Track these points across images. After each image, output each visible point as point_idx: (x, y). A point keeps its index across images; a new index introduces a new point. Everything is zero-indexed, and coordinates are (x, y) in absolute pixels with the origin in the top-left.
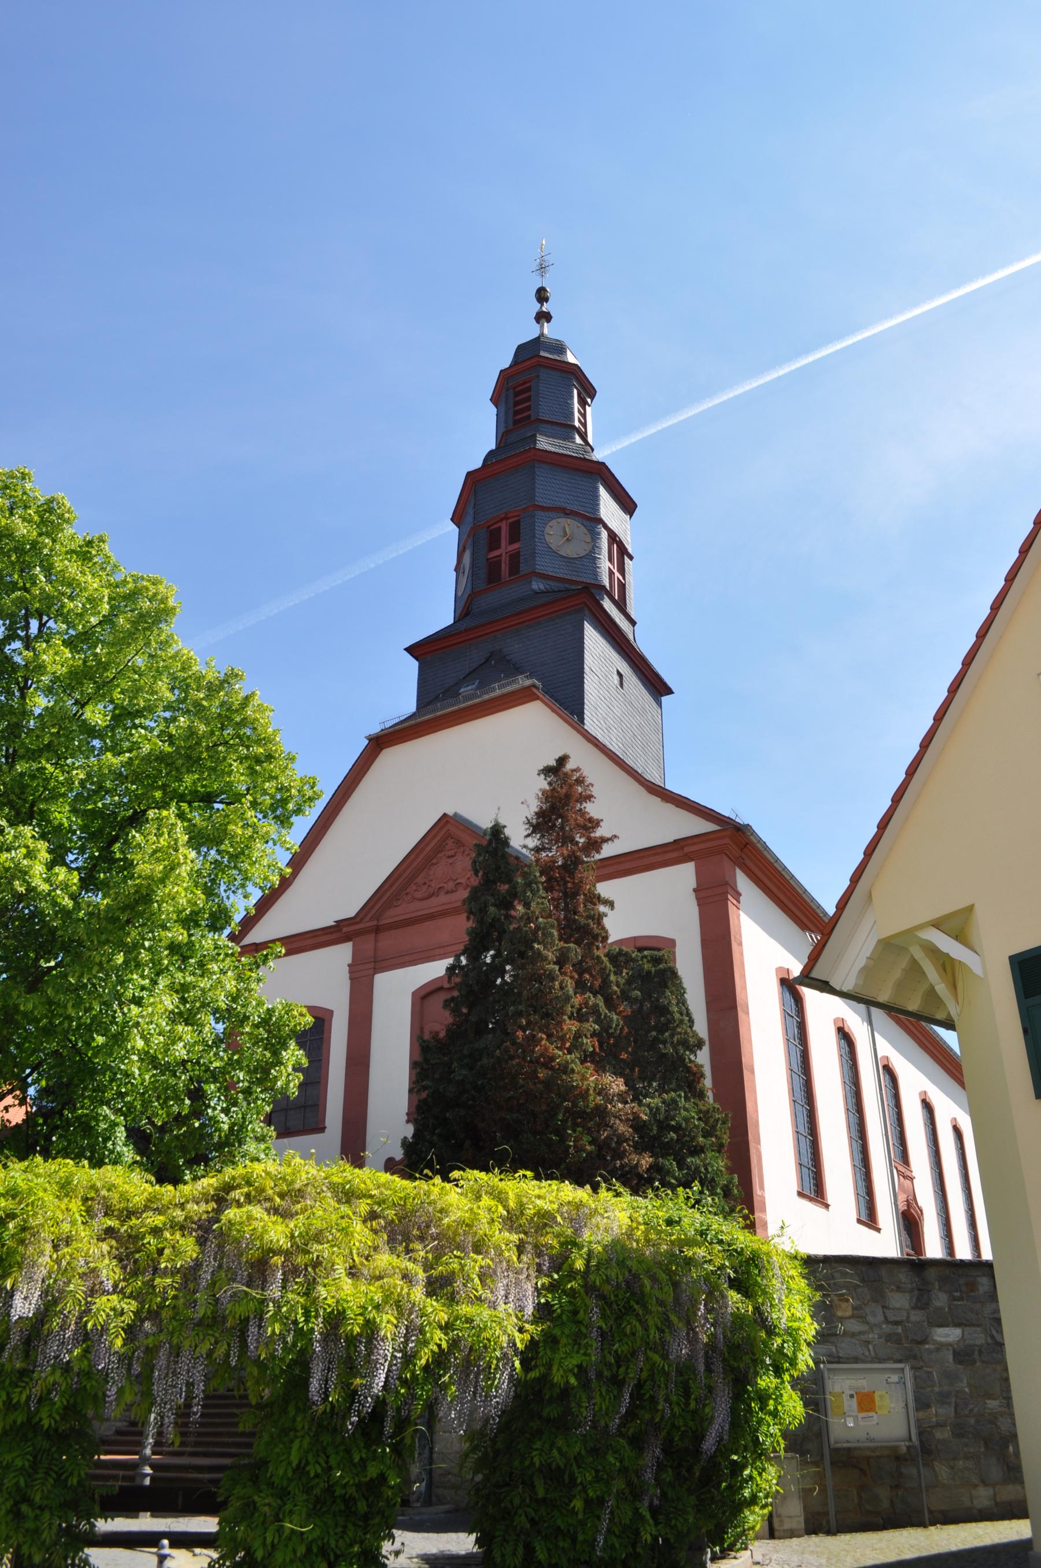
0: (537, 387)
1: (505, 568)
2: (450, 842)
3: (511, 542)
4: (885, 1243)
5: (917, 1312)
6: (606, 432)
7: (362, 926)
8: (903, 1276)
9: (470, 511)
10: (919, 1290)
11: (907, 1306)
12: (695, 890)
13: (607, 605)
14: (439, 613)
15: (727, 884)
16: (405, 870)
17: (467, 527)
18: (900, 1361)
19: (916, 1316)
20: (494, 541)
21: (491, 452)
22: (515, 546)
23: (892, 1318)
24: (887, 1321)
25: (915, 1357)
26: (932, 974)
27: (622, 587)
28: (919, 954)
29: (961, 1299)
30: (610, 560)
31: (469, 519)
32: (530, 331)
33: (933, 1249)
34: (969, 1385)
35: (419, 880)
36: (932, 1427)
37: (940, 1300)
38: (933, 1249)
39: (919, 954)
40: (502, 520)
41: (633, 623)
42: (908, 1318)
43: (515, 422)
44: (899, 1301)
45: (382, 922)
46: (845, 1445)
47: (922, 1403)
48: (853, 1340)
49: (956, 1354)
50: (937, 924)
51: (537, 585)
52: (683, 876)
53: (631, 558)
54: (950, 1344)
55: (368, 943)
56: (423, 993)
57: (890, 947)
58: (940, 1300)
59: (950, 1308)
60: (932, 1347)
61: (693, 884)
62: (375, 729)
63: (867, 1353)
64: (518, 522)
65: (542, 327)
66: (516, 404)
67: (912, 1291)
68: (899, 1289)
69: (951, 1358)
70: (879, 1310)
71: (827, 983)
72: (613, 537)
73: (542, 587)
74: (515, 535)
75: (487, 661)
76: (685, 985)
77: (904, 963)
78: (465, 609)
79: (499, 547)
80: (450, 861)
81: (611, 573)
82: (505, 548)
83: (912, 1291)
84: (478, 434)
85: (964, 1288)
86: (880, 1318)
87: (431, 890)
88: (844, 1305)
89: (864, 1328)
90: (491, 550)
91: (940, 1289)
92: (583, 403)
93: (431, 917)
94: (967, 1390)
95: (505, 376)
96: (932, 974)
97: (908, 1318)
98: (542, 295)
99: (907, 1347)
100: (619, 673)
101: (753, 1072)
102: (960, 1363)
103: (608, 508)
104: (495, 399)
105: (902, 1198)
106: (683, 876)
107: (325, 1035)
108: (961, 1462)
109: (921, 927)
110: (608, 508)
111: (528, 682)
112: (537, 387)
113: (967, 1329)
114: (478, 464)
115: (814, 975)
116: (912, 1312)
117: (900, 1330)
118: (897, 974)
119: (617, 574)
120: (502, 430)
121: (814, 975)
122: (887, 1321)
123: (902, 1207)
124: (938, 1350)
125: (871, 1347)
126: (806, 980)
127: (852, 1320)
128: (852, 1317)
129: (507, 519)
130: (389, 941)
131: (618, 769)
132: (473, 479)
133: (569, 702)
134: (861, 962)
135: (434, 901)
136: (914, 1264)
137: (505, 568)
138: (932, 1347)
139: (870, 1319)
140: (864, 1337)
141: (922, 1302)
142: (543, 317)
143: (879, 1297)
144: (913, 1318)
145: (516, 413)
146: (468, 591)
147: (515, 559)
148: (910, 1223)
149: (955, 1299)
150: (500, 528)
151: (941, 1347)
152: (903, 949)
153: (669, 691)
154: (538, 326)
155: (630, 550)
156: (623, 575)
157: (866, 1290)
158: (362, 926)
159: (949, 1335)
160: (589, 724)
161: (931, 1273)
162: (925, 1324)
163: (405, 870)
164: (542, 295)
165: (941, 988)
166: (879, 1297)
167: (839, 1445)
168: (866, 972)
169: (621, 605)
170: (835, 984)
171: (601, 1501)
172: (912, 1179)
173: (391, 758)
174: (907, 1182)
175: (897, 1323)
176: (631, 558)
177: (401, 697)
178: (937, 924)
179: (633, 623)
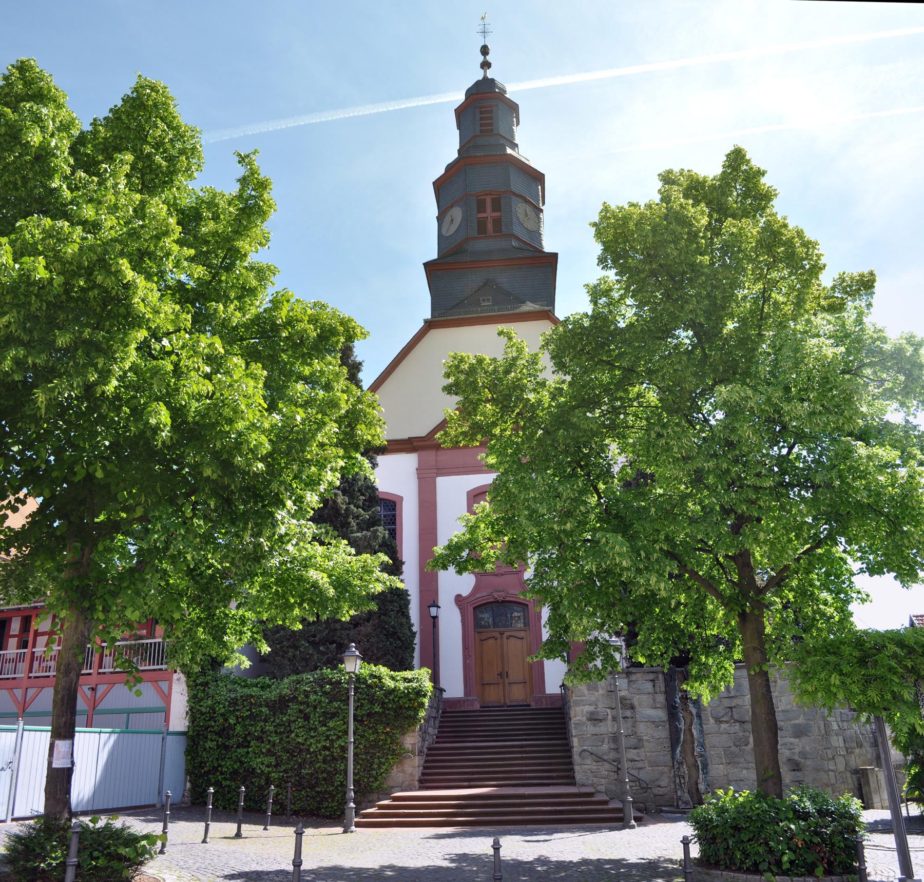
0: (485, 111)
1: (490, 226)
6: (530, 144)
32: (479, 75)
40: (486, 195)
43: (481, 131)
51: (514, 243)
55: (430, 455)
65: (485, 72)
76: (568, 860)
82: (489, 214)
98: (485, 50)
107: (397, 512)
112: (485, 111)
130: (445, 458)
137: (490, 226)
142: (486, 65)
147: (497, 222)
154: (482, 71)
164: (485, 50)
171: (826, 662)
177: (420, 304)
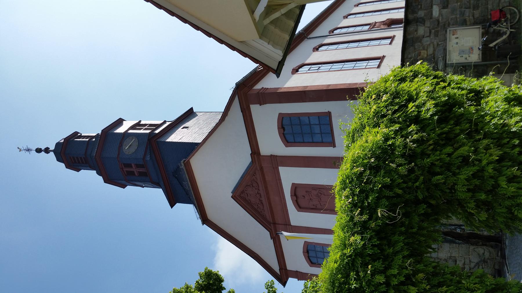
1: (141, 170)
2: (242, 195)
3: (132, 167)
4: (399, 33)
5: (426, 23)
6: (92, 129)
7: (273, 230)
8: (411, 28)
9: (120, 181)
10: (417, 22)
11: (424, 27)
12: (260, 105)
13: (157, 131)
14: (157, 195)
15: (258, 93)
16: (252, 212)
17: (127, 183)
18: (446, 31)
19: (428, 24)
20: (132, 173)
21: (97, 173)
22: (133, 165)
23: (428, 34)
24: (429, 36)
25: (444, 25)
26: (277, 15)
27: (151, 125)
28: (267, 21)
29: (421, 5)
30: (141, 129)
31: (124, 182)
33: (400, 15)
34: (457, 2)
35: (256, 207)
36: (474, 19)
37: (421, 14)
38: (400, 15)
39: (267, 21)
41: (165, 122)
42: (428, 27)
44: (421, 30)
45: (272, 222)
46: (481, 55)
47: (464, 23)
48: (437, 50)
49: (444, 8)
50: (252, 12)
51: (148, 158)
52: (255, 109)
53: (140, 121)
54: (440, 10)
56: (299, 208)
57: (263, 33)
58: (421, 14)
59: (425, 10)
60: (440, 18)
61: (258, 106)
62: (200, 221)
63: (442, 45)
64: (124, 164)
66: (79, 162)
67: (417, 25)
68: (416, 31)
69: (445, 10)
70: (425, 39)
71: (280, 62)
72: (133, 127)
73: (149, 156)
74: (130, 166)
75: (176, 178)
77: (272, 27)
78: (156, 184)
79: (133, 172)
80: (249, 195)
81: (146, 129)
83: (417, 25)
84: (90, 177)
85: (417, 4)
86: (428, 39)
87: (260, 203)
88: (422, 54)
89: (432, 45)
90: (135, 175)
91: (417, 13)
92: (81, 137)
93: (270, 204)
94: (459, 4)
95: (68, 167)
96: (277, 15)
97: (428, 27)
99: (441, 29)
100: (183, 128)
101: (329, 85)
102: (448, 6)
103: (121, 130)
104: (78, 170)
105: (382, 27)
106: (255, 109)
108: (489, 7)
109: (254, 20)
110: (121, 130)
111: (183, 164)
113: (433, 3)
114: (101, 178)
115: (275, 68)
116: (426, 25)
117: (433, 31)
118: (277, 31)
119: (146, 127)
120: (89, 168)
121: (275, 68)
122: (429, 36)
123: (386, 27)
124: (442, 15)
125: (440, 43)
126: (278, 72)
127: (428, 50)
128: (427, 50)
129: (122, 168)
131: (221, 125)
132: (107, 180)
133: (190, 148)
134: (270, 47)
135: (264, 202)
136: (407, 22)
137: (141, 170)
138: (440, 18)
139: (428, 43)
140: (436, 45)
141: (421, 21)
143: (419, 39)
144: (428, 25)
145: (83, 163)
146: (150, 183)
147: (137, 166)
148: (391, 23)
149: (421, 8)
150: (126, 171)
151: (440, 14)
152: (265, 27)
153: (192, 109)
155: (137, 122)
156: (147, 125)
157: (416, 44)
158: (273, 230)
159: (436, 11)
160: (199, 140)
161: (411, 17)
162: (431, 20)
163: (252, 212)
165: (284, 11)
166: (419, 39)
167: (481, 58)
168: (275, 44)
169: (158, 126)
170: (280, 58)
172: (376, 23)
173: (211, 215)
174: (377, 24)
175: (430, 32)
176: (140, 121)
177: (187, 211)
178: (252, 12)
179: (165, 122)
